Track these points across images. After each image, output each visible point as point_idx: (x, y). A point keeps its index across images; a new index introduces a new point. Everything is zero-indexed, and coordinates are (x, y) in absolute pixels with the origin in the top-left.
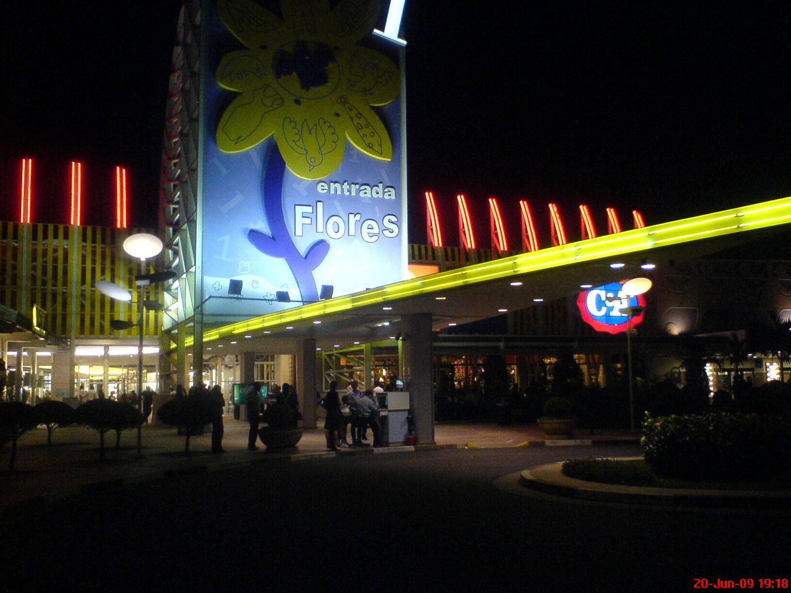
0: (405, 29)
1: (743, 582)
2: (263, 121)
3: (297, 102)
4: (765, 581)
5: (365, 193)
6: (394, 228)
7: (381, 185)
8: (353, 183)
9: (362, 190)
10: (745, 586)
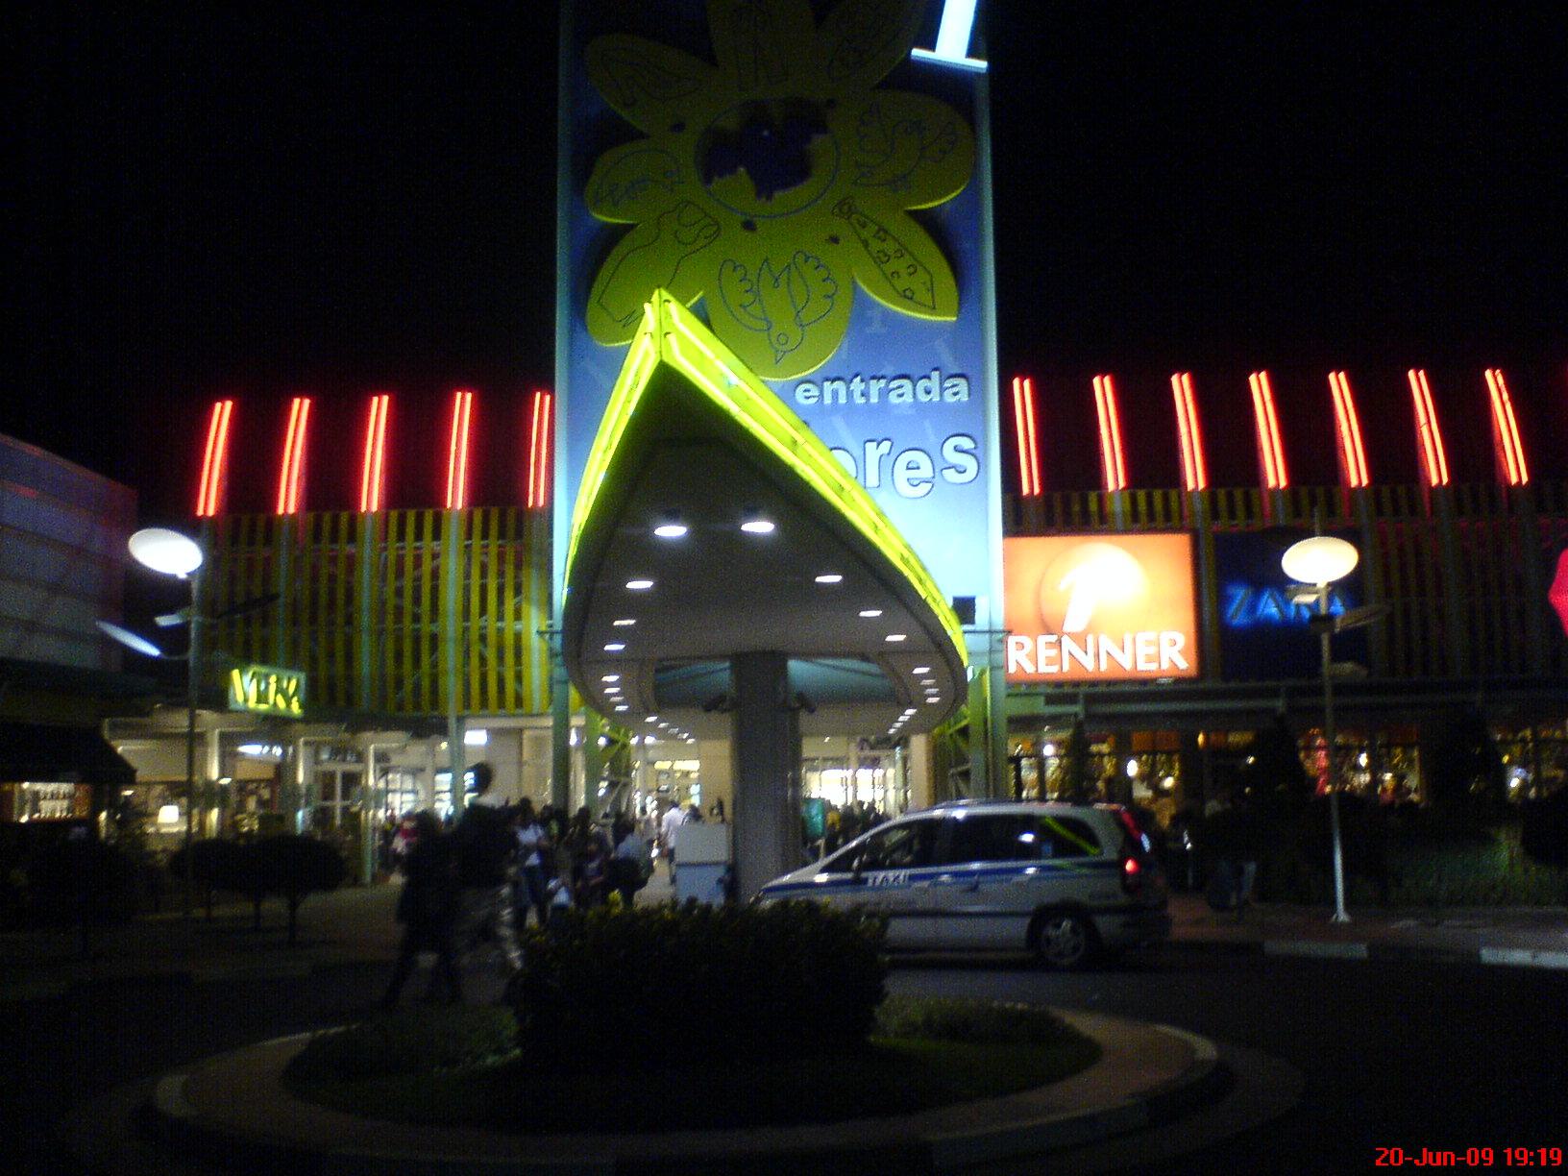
0: (985, 36)
1: (1473, 1154)
2: (677, 278)
3: (749, 226)
5: (901, 395)
6: (970, 463)
7: (935, 375)
8: (873, 378)
9: (894, 389)
10: (1477, 1162)
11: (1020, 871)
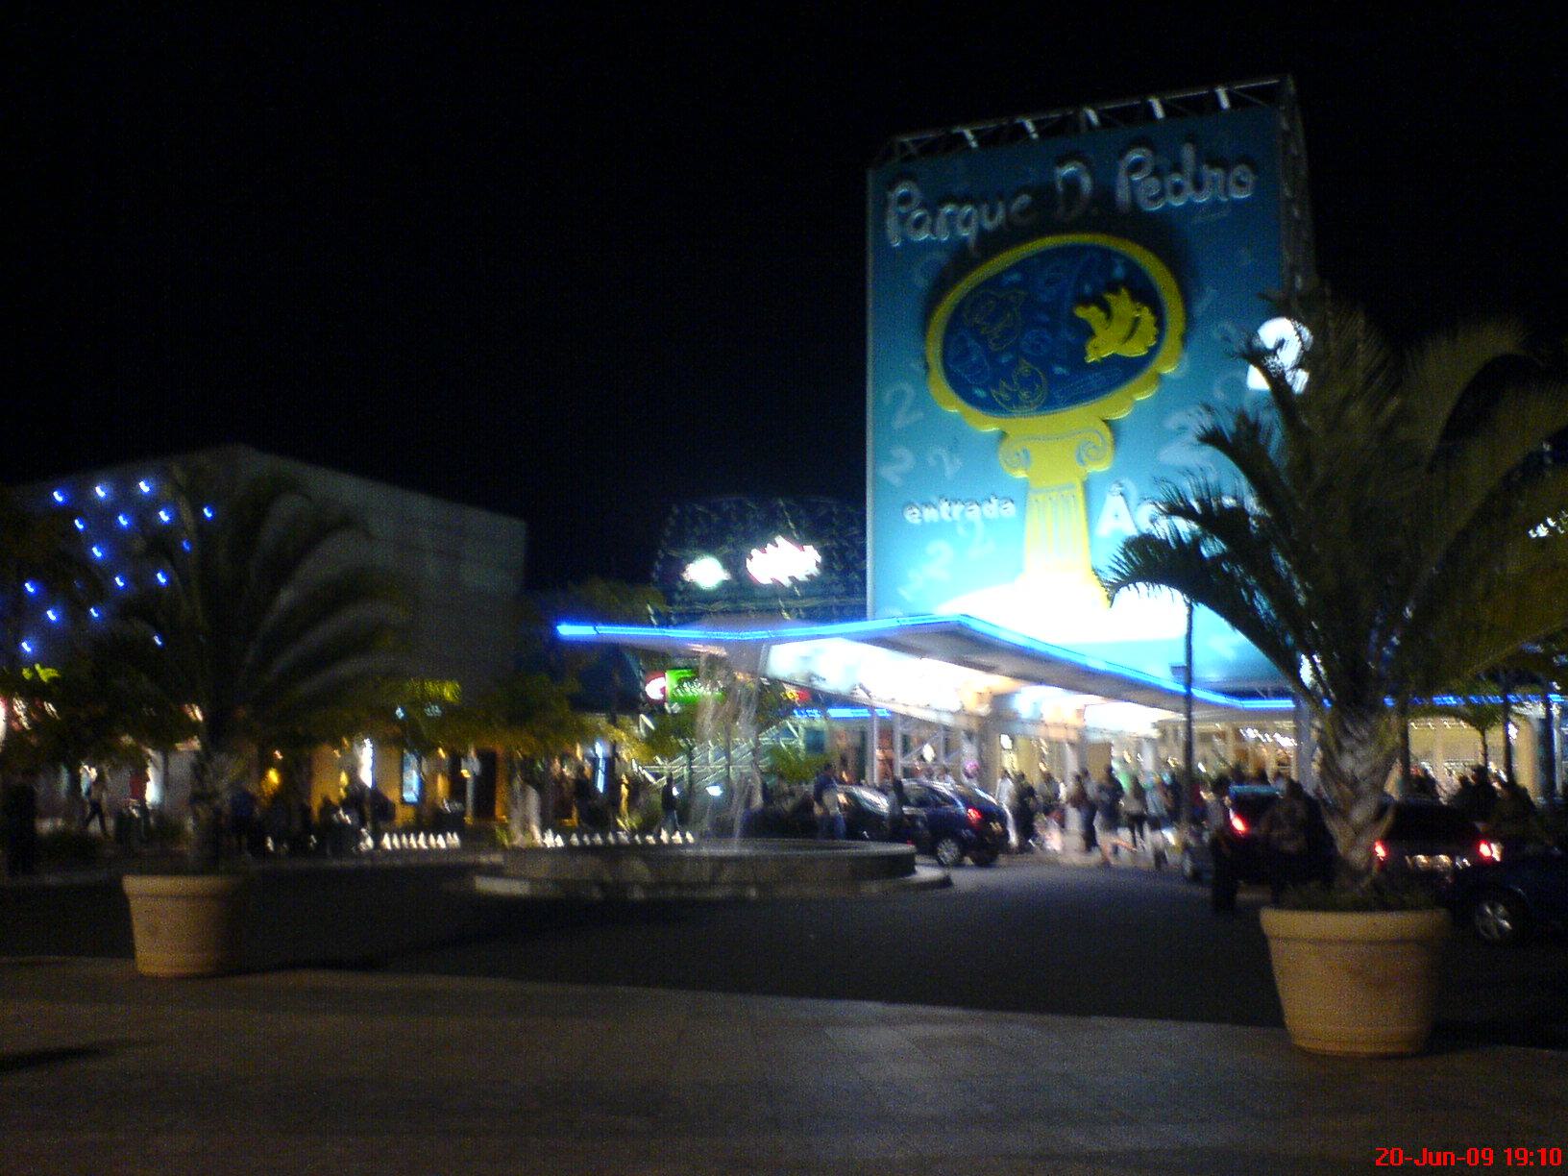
1: (1555, 1154)
4: (1483, 1153)
10: (1477, 1162)
11: (905, 865)
